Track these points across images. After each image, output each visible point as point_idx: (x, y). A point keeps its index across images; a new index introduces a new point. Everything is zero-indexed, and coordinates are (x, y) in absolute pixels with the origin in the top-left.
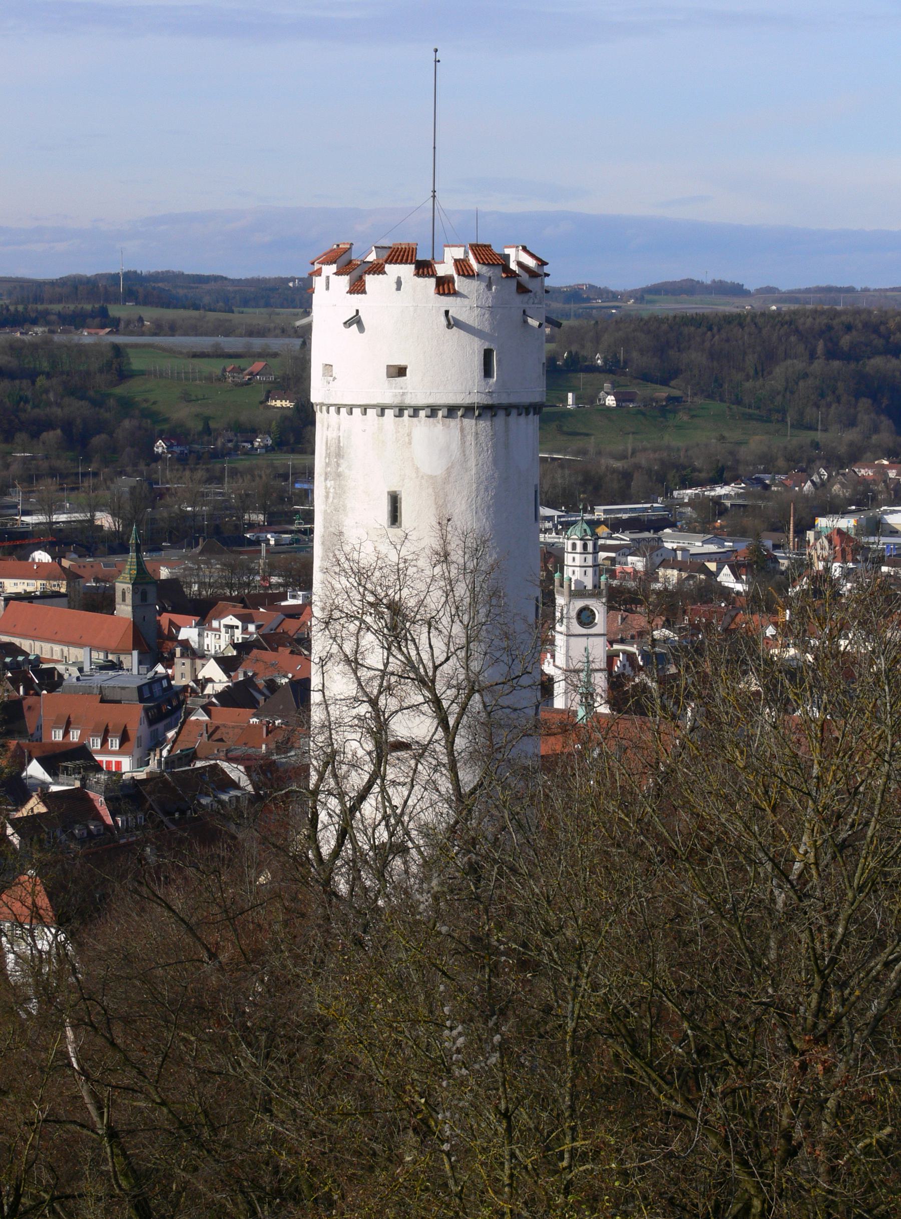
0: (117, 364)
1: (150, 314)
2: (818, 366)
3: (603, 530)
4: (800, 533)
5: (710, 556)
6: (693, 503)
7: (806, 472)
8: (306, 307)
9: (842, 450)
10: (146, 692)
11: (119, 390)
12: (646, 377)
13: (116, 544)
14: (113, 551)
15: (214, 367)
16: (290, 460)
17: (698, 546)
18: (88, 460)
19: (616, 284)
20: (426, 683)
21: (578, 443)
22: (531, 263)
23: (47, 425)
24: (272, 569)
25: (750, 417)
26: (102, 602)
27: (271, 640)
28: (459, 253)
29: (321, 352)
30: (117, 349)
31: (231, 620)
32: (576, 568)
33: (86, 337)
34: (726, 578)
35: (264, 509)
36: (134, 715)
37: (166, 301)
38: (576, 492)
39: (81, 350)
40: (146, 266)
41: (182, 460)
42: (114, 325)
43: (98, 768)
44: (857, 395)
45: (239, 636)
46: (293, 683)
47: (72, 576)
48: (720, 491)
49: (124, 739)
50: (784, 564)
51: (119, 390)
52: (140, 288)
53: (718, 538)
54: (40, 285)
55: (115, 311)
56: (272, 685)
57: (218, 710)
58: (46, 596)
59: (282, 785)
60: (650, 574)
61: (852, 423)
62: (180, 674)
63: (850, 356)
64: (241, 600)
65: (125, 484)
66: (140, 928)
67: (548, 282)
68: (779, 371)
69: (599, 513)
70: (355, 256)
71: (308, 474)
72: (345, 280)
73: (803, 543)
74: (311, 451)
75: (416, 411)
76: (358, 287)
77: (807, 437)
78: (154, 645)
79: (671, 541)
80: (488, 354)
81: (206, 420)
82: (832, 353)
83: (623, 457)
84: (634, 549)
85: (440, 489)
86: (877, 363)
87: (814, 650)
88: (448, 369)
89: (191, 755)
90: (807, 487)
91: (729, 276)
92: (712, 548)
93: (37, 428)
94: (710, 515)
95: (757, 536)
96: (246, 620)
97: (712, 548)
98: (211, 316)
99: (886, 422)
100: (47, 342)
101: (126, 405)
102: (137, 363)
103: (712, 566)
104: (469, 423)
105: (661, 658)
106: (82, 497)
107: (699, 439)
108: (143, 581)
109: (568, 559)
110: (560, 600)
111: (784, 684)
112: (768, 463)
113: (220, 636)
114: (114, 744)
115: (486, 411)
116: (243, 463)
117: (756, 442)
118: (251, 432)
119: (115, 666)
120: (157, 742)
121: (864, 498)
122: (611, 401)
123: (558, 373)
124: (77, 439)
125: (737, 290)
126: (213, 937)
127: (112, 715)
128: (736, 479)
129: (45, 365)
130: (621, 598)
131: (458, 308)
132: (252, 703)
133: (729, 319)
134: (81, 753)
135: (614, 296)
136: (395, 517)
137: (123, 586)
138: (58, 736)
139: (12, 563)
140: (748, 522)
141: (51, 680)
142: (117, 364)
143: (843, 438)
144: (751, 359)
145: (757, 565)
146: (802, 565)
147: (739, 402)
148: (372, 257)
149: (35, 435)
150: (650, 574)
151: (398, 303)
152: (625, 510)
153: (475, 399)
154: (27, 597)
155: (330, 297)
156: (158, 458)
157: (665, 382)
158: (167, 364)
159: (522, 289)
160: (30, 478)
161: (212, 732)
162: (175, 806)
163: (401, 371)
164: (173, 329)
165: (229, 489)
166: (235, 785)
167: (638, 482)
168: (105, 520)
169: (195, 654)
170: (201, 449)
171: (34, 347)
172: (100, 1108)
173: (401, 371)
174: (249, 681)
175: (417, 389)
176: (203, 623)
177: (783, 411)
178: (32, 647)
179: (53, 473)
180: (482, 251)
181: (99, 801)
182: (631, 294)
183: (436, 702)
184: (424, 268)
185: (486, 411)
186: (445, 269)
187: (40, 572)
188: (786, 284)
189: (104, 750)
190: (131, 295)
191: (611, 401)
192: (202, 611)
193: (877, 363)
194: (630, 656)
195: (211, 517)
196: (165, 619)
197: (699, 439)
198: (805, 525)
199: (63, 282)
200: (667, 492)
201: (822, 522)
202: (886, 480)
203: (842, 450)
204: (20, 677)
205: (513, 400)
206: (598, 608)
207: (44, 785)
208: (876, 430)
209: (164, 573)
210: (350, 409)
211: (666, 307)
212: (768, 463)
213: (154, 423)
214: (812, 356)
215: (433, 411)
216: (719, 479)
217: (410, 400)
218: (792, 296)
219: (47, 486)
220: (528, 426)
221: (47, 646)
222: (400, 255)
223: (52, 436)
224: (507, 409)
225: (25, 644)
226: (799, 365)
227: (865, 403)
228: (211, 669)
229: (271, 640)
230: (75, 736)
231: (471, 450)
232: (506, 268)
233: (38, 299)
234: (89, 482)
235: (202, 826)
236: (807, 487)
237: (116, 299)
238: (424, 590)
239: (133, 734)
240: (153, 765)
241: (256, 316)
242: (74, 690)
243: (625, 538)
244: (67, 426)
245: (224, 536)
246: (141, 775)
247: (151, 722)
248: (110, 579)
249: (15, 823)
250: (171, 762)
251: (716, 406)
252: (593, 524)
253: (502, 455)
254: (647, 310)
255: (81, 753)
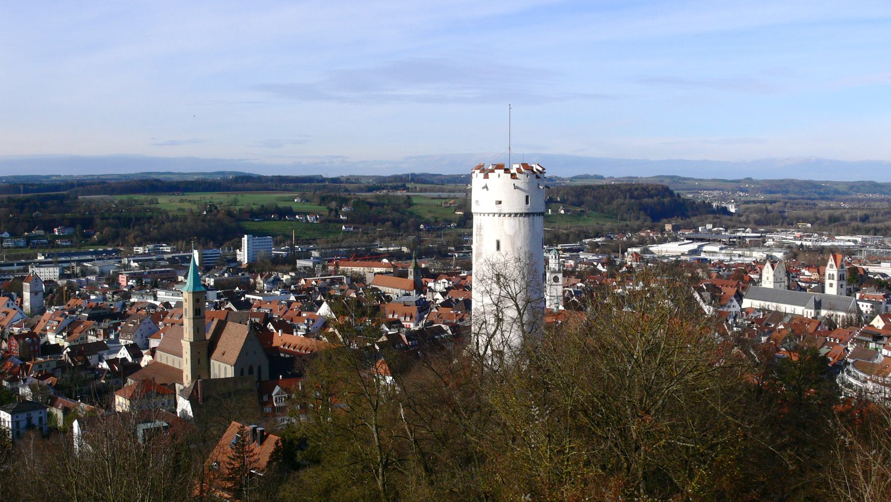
0: (408, 201)
1: (419, 186)
2: (627, 201)
3: (561, 252)
4: (623, 253)
5: (594, 260)
6: (589, 243)
7: (624, 234)
8: (470, 183)
9: (636, 227)
10: (417, 303)
11: (409, 209)
12: (573, 204)
13: (408, 257)
14: (407, 259)
15: (438, 202)
16: (467, 231)
17: (591, 257)
18: (399, 231)
19: (564, 176)
20: (514, 299)
21: (553, 225)
22: (540, 169)
23: (388, 220)
24: (456, 265)
25: (606, 217)
26: (404, 275)
27: (457, 287)
28: (518, 166)
29: (475, 196)
30: (408, 196)
31: (444, 280)
32: (553, 264)
33: (399, 193)
34: (600, 267)
35: (454, 246)
36: (414, 310)
37: (424, 182)
38: (551, 240)
39: (398, 197)
40: (417, 171)
41: (429, 231)
42: (408, 189)
43: (403, 326)
44: (640, 210)
45: (447, 285)
46: (464, 300)
47: (394, 267)
48: (597, 240)
49: (411, 317)
50: (618, 263)
51: (409, 209)
52: (415, 178)
53: (597, 254)
54: (385, 178)
55: (408, 185)
56: (457, 301)
57: (441, 308)
58: (386, 273)
59: (461, 333)
60: (576, 266)
61: (638, 219)
62: (429, 297)
63: (637, 198)
64: (447, 274)
65: (411, 238)
66: (423, 376)
67: (546, 175)
68: (615, 202)
69: (559, 247)
70: (485, 167)
71: (471, 235)
72: (482, 174)
73: (624, 257)
74: (472, 227)
75: (505, 215)
76: (486, 177)
77: (624, 223)
78: (420, 288)
79: (582, 255)
80: (527, 197)
81: (436, 218)
82: (631, 197)
83: (566, 229)
84: (570, 258)
85: (513, 239)
86: (645, 200)
87: (255, 279)
88: (515, 202)
89: (432, 323)
90: (625, 239)
91: (599, 173)
92: (595, 258)
93: (384, 221)
94: (594, 248)
95: (609, 254)
96: (449, 280)
97: (595, 258)
98: (438, 186)
99: (649, 219)
100: (387, 195)
101: (411, 214)
102: (415, 201)
103: (595, 263)
104: (521, 218)
105: (580, 292)
106: (397, 242)
107: (591, 223)
108: (417, 268)
109: (550, 261)
110: (548, 275)
111: (620, 301)
112: (612, 231)
113: (441, 285)
114: (408, 319)
115: (527, 215)
116: (447, 232)
117: (608, 224)
118: (450, 222)
119: (408, 295)
120: (421, 318)
121: (642, 242)
122: (562, 212)
123: (549, 202)
124: (396, 224)
125: (602, 178)
126: (446, 379)
127: (407, 310)
128: (602, 236)
129: (387, 202)
130: (566, 274)
131: (518, 183)
132: (451, 306)
133: (599, 187)
134: (398, 322)
135: (563, 179)
136: (498, 248)
137: (411, 270)
138: (390, 316)
139: (376, 263)
140: (606, 249)
141: (389, 299)
142: (408, 201)
143: (635, 224)
144: (606, 199)
145: (609, 263)
146: (623, 264)
147: (603, 212)
148: (490, 168)
149: (383, 223)
150: (576, 266)
151: (499, 182)
152: (567, 246)
153: (523, 211)
154: (378, 273)
155: (478, 180)
156: (421, 230)
157: (579, 206)
158: (424, 201)
159: (537, 177)
160: (382, 237)
161: (439, 315)
162: (427, 338)
163: (500, 203)
164: (425, 191)
165: (443, 240)
166: (446, 332)
167: (571, 236)
168: (405, 249)
169: (433, 291)
170: (434, 227)
171: (383, 196)
172: (411, 432)
173: (500, 203)
174: (450, 300)
175: (505, 208)
176: (435, 281)
177: (616, 215)
178: (383, 289)
179: (389, 235)
180: (525, 165)
181: (404, 336)
182: (569, 179)
183: (517, 305)
184: (507, 171)
185: (527, 215)
186: (513, 171)
187: (385, 266)
188: (616, 176)
189: (405, 321)
190: (413, 180)
191: (562, 212)
192: (435, 277)
193: (645, 200)
194: (570, 292)
195: (438, 248)
196: (423, 280)
197: (591, 223)
198: (624, 251)
199: (392, 177)
200: (581, 240)
201: (629, 250)
202: (649, 236)
203: (636, 227)
204: (379, 298)
205: (535, 211)
206: (560, 276)
207: (387, 332)
208: (646, 221)
209: (423, 266)
210: (484, 214)
211: (579, 183)
212: (612, 231)
213: (419, 219)
214: (625, 198)
215: (510, 215)
216: (597, 236)
217: (503, 211)
218: (618, 180)
219: (387, 239)
220: (539, 220)
221: (767, 303)
222: (499, 167)
223: (389, 224)
224: (533, 214)
225: (380, 288)
226: (621, 201)
227: (642, 212)
228: (438, 296)
229: (457, 287)
230: (396, 316)
231: (522, 227)
232: (532, 171)
233: (384, 182)
234: (400, 238)
235: (440, 343)
236: (625, 239)
237: (409, 182)
238: (512, 270)
239: (414, 315)
240: (420, 326)
241: (451, 186)
242: (396, 302)
243: (567, 255)
244: (393, 221)
245: (442, 254)
246: (417, 329)
247: (420, 312)
248: (407, 267)
249: (378, 344)
250: (426, 325)
251: (595, 213)
252: (558, 250)
253: (532, 227)
254: (573, 184)
255: (398, 322)
